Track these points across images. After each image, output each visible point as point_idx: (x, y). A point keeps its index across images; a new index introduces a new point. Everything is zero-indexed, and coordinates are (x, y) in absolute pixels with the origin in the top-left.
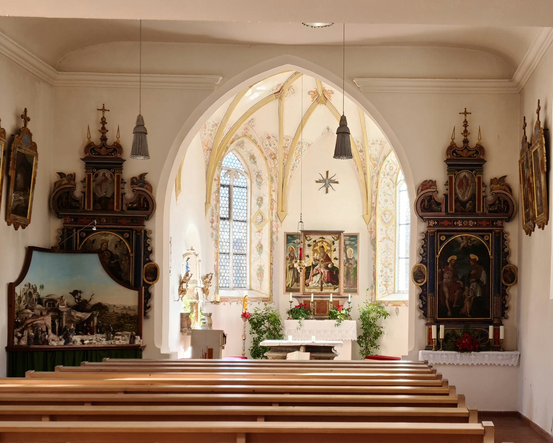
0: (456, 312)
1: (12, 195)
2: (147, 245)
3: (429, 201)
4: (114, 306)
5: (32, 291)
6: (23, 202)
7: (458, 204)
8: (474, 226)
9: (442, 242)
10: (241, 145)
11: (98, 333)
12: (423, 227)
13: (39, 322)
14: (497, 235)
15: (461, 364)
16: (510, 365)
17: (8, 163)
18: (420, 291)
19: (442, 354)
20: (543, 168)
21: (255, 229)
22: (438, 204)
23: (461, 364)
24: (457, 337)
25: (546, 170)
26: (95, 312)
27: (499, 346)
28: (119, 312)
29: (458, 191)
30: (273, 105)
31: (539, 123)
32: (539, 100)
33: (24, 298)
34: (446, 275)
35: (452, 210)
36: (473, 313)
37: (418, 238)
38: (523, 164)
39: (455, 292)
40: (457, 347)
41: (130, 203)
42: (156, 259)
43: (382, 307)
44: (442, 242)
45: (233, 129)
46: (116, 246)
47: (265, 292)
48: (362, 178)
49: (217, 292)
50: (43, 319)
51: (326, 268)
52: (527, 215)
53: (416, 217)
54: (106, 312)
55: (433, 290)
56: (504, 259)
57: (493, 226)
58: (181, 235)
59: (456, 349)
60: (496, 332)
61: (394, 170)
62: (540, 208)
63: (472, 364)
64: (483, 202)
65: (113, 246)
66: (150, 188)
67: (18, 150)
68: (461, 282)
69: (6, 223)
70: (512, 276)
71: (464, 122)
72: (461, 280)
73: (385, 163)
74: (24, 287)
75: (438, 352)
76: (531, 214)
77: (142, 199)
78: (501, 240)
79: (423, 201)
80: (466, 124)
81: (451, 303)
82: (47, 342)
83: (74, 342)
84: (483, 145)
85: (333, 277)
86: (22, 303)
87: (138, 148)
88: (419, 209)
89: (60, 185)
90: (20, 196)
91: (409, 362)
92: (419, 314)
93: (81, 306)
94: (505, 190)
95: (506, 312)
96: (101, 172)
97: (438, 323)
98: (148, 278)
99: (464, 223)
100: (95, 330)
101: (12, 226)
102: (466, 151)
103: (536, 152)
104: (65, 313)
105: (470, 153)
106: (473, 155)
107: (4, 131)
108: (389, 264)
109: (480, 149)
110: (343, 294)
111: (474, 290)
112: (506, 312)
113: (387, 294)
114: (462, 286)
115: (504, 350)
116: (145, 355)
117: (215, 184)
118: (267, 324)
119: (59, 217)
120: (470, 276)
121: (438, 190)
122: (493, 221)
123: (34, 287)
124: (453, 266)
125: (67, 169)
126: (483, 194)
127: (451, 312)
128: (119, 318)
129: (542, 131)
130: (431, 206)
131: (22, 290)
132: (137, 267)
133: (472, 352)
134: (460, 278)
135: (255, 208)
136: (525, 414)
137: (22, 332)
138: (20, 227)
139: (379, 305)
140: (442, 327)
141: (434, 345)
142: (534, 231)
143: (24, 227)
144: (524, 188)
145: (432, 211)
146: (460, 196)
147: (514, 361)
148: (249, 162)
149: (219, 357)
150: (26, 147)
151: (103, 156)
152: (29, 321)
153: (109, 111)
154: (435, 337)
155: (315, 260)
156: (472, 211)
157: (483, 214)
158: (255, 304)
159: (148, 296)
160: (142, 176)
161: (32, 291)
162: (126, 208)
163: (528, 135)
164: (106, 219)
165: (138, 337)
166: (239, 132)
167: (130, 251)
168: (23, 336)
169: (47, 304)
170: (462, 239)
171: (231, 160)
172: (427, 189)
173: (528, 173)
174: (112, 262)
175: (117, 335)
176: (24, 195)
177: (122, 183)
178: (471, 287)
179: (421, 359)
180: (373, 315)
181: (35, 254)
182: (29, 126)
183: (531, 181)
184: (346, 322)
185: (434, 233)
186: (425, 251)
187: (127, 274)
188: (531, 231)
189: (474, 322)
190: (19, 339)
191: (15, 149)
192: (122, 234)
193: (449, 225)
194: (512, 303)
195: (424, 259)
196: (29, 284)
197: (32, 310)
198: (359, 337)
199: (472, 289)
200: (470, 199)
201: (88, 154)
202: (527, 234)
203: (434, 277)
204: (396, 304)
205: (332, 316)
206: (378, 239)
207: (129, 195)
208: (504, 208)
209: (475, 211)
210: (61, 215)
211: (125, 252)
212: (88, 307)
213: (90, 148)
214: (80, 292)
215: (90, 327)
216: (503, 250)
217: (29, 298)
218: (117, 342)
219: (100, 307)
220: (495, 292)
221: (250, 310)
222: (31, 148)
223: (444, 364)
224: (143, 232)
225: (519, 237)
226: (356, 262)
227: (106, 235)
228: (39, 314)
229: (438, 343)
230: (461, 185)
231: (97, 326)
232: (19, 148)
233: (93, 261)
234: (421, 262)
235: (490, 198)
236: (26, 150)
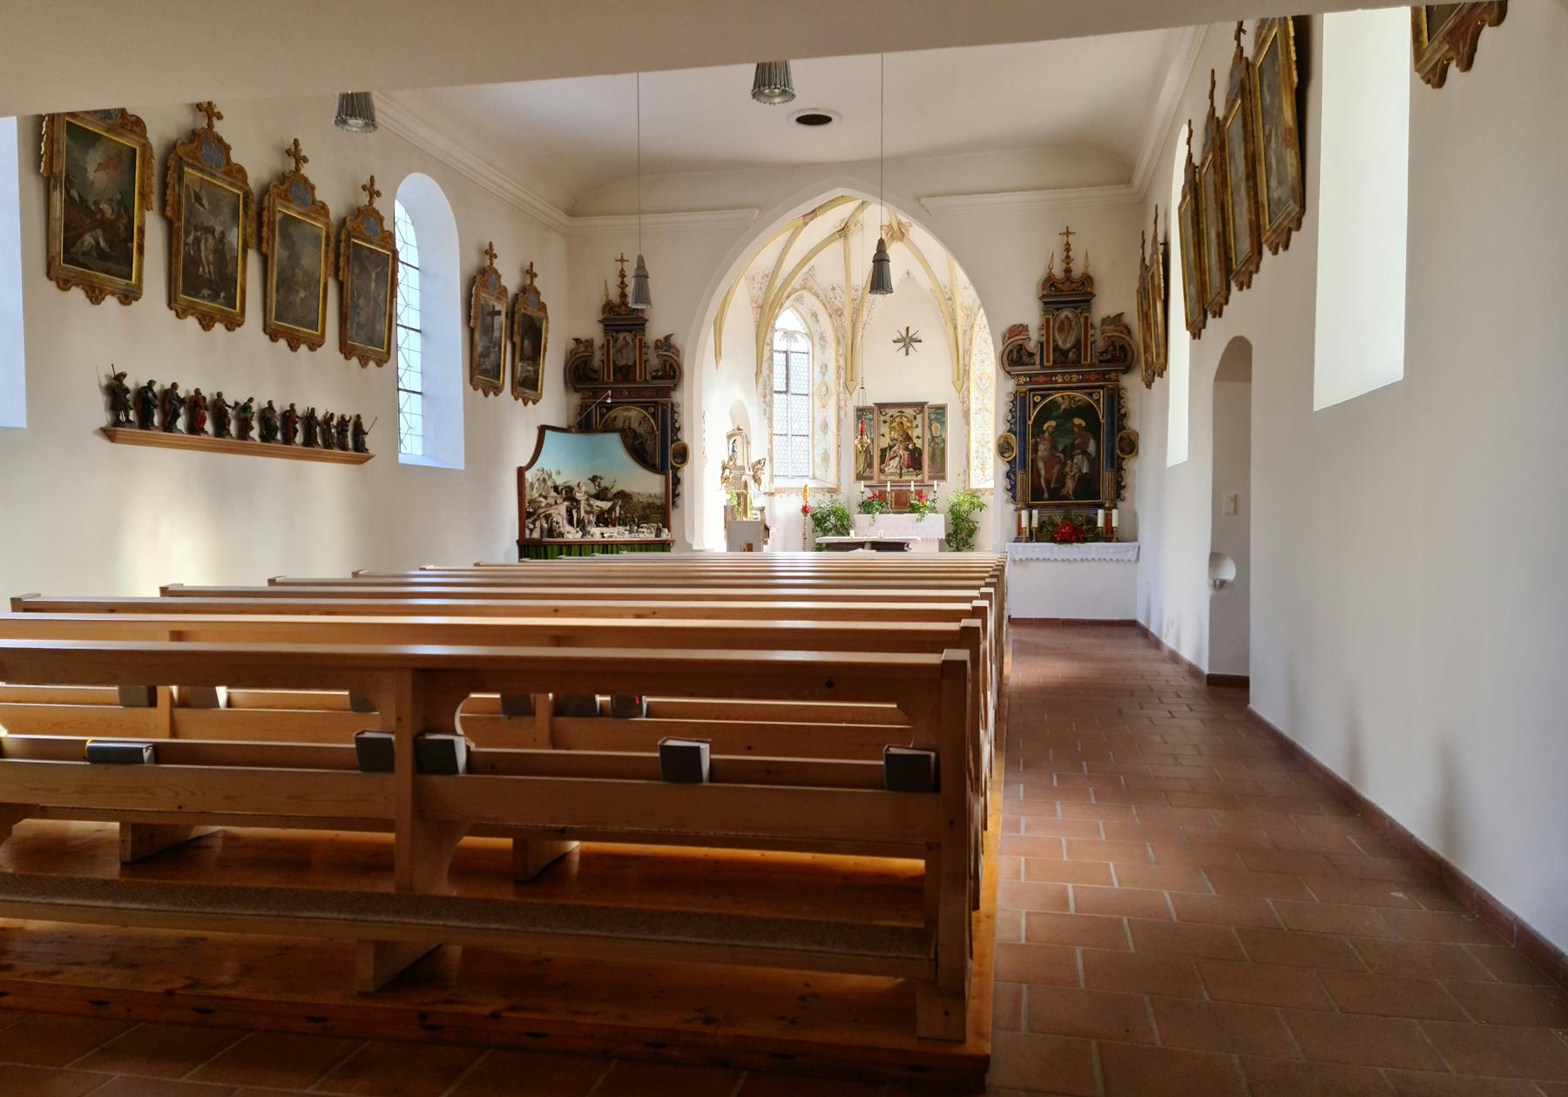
0: (1056, 494)
2: (674, 421)
3: (1019, 352)
9: (1036, 404)
10: (800, 299)
12: (1010, 386)
18: (1006, 468)
21: (818, 404)
22: (1031, 355)
30: (838, 246)
34: (1041, 447)
37: (1006, 399)
42: (685, 437)
44: (1036, 404)
45: (787, 281)
47: (831, 482)
48: (951, 332)
49: (772, 480)
51: (907, 449)
53: (1002, 374)
55: (1024, 466)
58: (714, 407)
59: (1053, 540)
60: (1108, 518)
66: (677, 352)
70: (1130, 446)
78: (1116, 399)
80: (1068, 248)
81: (1048, 482)
82: (562, 535)
85: (915, 461)
96: (621, 336)
97: (1030, 508)
109: (1087, 280)
110: (927, 482)
111: (1081, 465)
117: (767, 348)
118: (833, 519)
119: (576, 390)
120: (1073, 446)
122: (1104, 373)
124: (1051, 434)
125: (584, 334)
126: (1090, 339)
128: (644, 508)
132: (662, 449)
135: (818, 378)
136: (1153, 630)
137: (534, 523)
139: (974, 494)
140: (1035, 512)
141: (1036, 535)
143: (535, 402)
147: (1131, 555)
148: (810, 320)
149: (760, 550)
151: (623, 318)
155: (893, 439)
156: (1077, 362)
158: (820, 496)
159: (677, 481)
160: (667, 338)
166: (797, 282)
171: (787, 319)
180: (966, 507)
181: (548, 433)
182: (537, 283)
184: (929, 516)
187: (653, 456)
192: (646, 408)
198: (948, 535)
205: (913, 509)
206: (972, 411)
213: (608, 307)
219: (622, 495)
221: (812, 503)
226: (944, 441)
230: (1061, 330)
233: (613, 442)
235: (1101, 344)
236: (533, 311)
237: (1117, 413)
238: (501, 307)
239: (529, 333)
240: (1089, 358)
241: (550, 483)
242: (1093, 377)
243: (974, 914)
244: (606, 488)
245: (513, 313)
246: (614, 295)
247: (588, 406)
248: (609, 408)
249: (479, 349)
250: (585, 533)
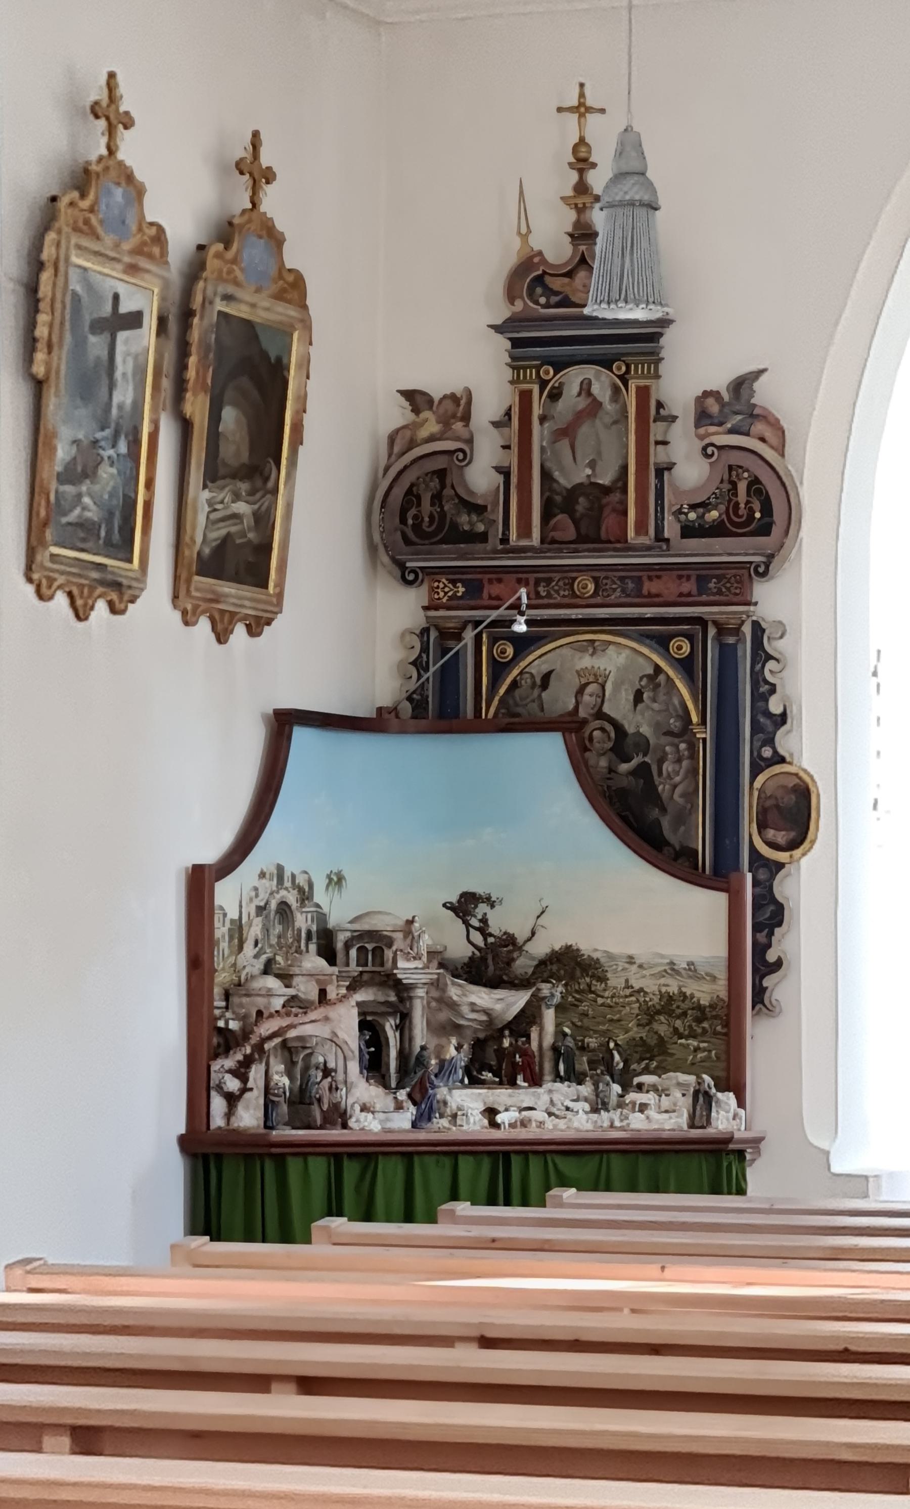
1: (200, 497)
2: (764, 691)
4: (631, 960)
5: (292, 898)
6: (248, 521)
11: (558, 1078)
13: (307, 1030)
17: (182, 366)
26: (545, 989)
28: (651, 986)
33: (255, 930)
41: (693, 507)
46: (638, 697)
50: (327, 1019)
54: (598, 986)
65: (626, 696)
67: (220, 306)
69: (177, 615)
74: (256, 882)
77: (742, 487)
82: (338, 1116)
83: (454, 1116)
86: (249, 949)
87: (617, 270)
89: (412, 444)
90: (237, 497)
93: (491, 963)
96: (574, 377)
98: (771, 833)
100: (548, 1066)
101: (204, 624)
104: (420, 992)
107: (159, 236)
116: (757, 1178)
119: (408, 578)
123: (301, 880)
128: (650, 1015)
131: (247, 893)
138: (240, 630)
150: (258, 290)
151: (566, 323)
152: (266, 1028)
153: (602, 111)
159: (771, 915)
160: (742, 385)
161: (292, 898)
162: (678, 527)
164: (596, 580)
165: (729, 1098)
167: (695, 718)
168: (245, 1090)
169: (353, 953)
174: (624, 767)
175: (640, 1087)
176: (252, 493)
177: (658, 418)
181: (301, 736)
182: (272, 202)
187: (683, 818)
190: (232, 1100)
191: (207, 302)
192: (662, 643)
196: (280, 869)
197: (286, 978)
201: (519, 306)
207: (691, 472)
210: (413, 571)
211: (675, 724)
212: (523, 965)
214: (489, 901)
215: (526, 1054)
217: (278, 929)
218: (638, 1123)
219: (568, 965)
222: (279, 296)
224: (747, 629)
227: (593, 648)
228: (314, 995)
231: (555, 1049)
232: (228, 298)
236: (258, 307)
238: (143, 297)
239: (246, 385)
241: (303, 921)
242: (668, 587)
244: (509, 940)
245: (187, 315)
246: (552, 239)
247: (451, 635)
248: (523, 644)
249: (63, 453)
250: (426, 1108)
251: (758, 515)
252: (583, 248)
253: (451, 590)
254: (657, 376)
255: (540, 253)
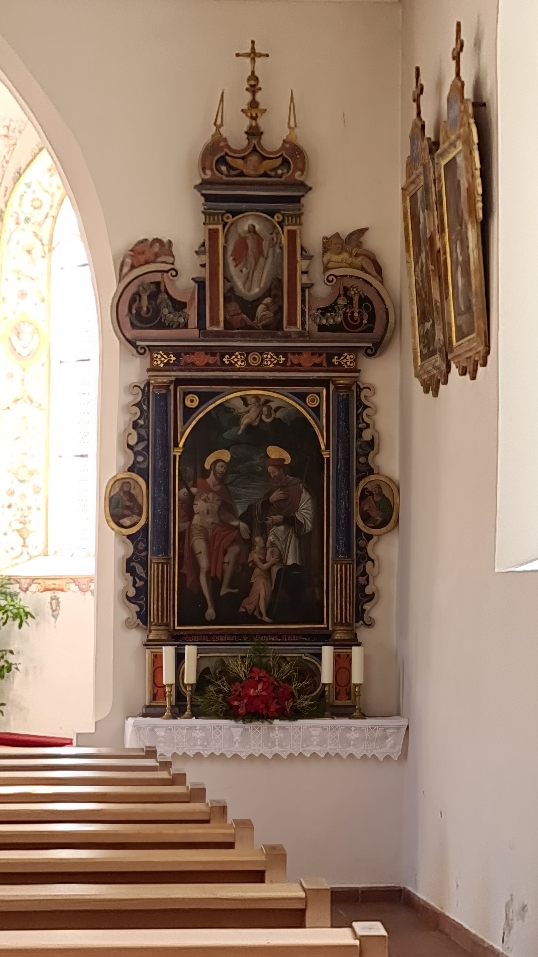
0: (230, 609)
3: (153, 297)
7: (234, 306)
8: (279, 367)
9: (188, 413)
12: (136, 370)
14: (342, 393)
15: (244, 756)
16: (381, 757)
18: (128, 549)
19: (193, 728)
20: (472, 210)
22: (179, 306)
23: (244, 756)
24: (234, 680)
25: (480, 215)
27: (349, 703)
29: (232, 269)
31: (459, 85)
32: (459, 25)
34: (199, 506)
35: (218, 323)
36: (276, 612)
37: (121, 401)
38: (413, 198)
39: (225, 552)
40: (232, 707)
43: (13, 596)
44: (188, 413)
52: (427, 339)
53: (115, 342)
55: (164, 548)
56: (362, 460)
57: (331, 367)
59: (229, 713)
60: (342, 665)
61: (46, 208)
62: (462, 319)
63: (276, 756)
64: (303, 302)
68: (243, 525)
70: (384, 509)
71: (249, 80)
72: (242, 518)
73: (21, 187)
75: (180, 721)
76: (439, 335)
78: (352, 406)
79: (136, 297)
81: (215, 583)
84: (301, 143)
88: (126, 321)
91: (104, 751)
92: (124, 615)
94: (363, 269)
95: (367, 607)
97: (178, 640)
99: (250, 360)
102: (254, 158)
103: (451, 165)
105: (267, 165)
106: (275, 170)
108: (31, 473)
109: (293, 155)
112: (367, 607)
113: (25, 557)
114: (246, 536)
115: (363, 716)
120: (267, 505)
121: (177, 266)
124: (221, 479)
127: (216, 610)
129: (470, 110)
130: (157, 311)
133: (276, 722)
134: (240, 512)
136: (423, 894)
141: (184, 703)
142: (446, 382)
144: (416, 263)
145: (162, 326)
146: (239, 284)
147: (391, 746)
154: (172, 681)
156: (275, 327)
157: (303, 335)
163: (428, 118)
167: (323, 447)
170: (246, 404)
172: (147, 263)
173: (428, 221)
178: (271, 538)
179: (131, 742)
183: (439, 245)
185: (167, 388)
186: (141, 438)
188: (438, 381)
189: (280, 636)
193: (208, 364)
194: (384, 582)
195: (140, 459)
199: (273, 544)
200: (267, 293)
201: (209, 174)
202: (426, 391)
203: (168, 510)
204: (53, 586)
208: (362, 320)
209: (280, 327)
210: (142, 348)
216: (359, 435)
220: (337, 553)
223: (198, 755)
225: (401, 397)
229: (180, 696)
230: (240, 254)
234: (131, 469)
235: (322, 291)
237: (357, 443)
240: (301, 322)
243: (203, 352)
251: (365, 322)
252: (255, 141)
253: (233, 360)
254: (301, 224)
255: (225, 140)
